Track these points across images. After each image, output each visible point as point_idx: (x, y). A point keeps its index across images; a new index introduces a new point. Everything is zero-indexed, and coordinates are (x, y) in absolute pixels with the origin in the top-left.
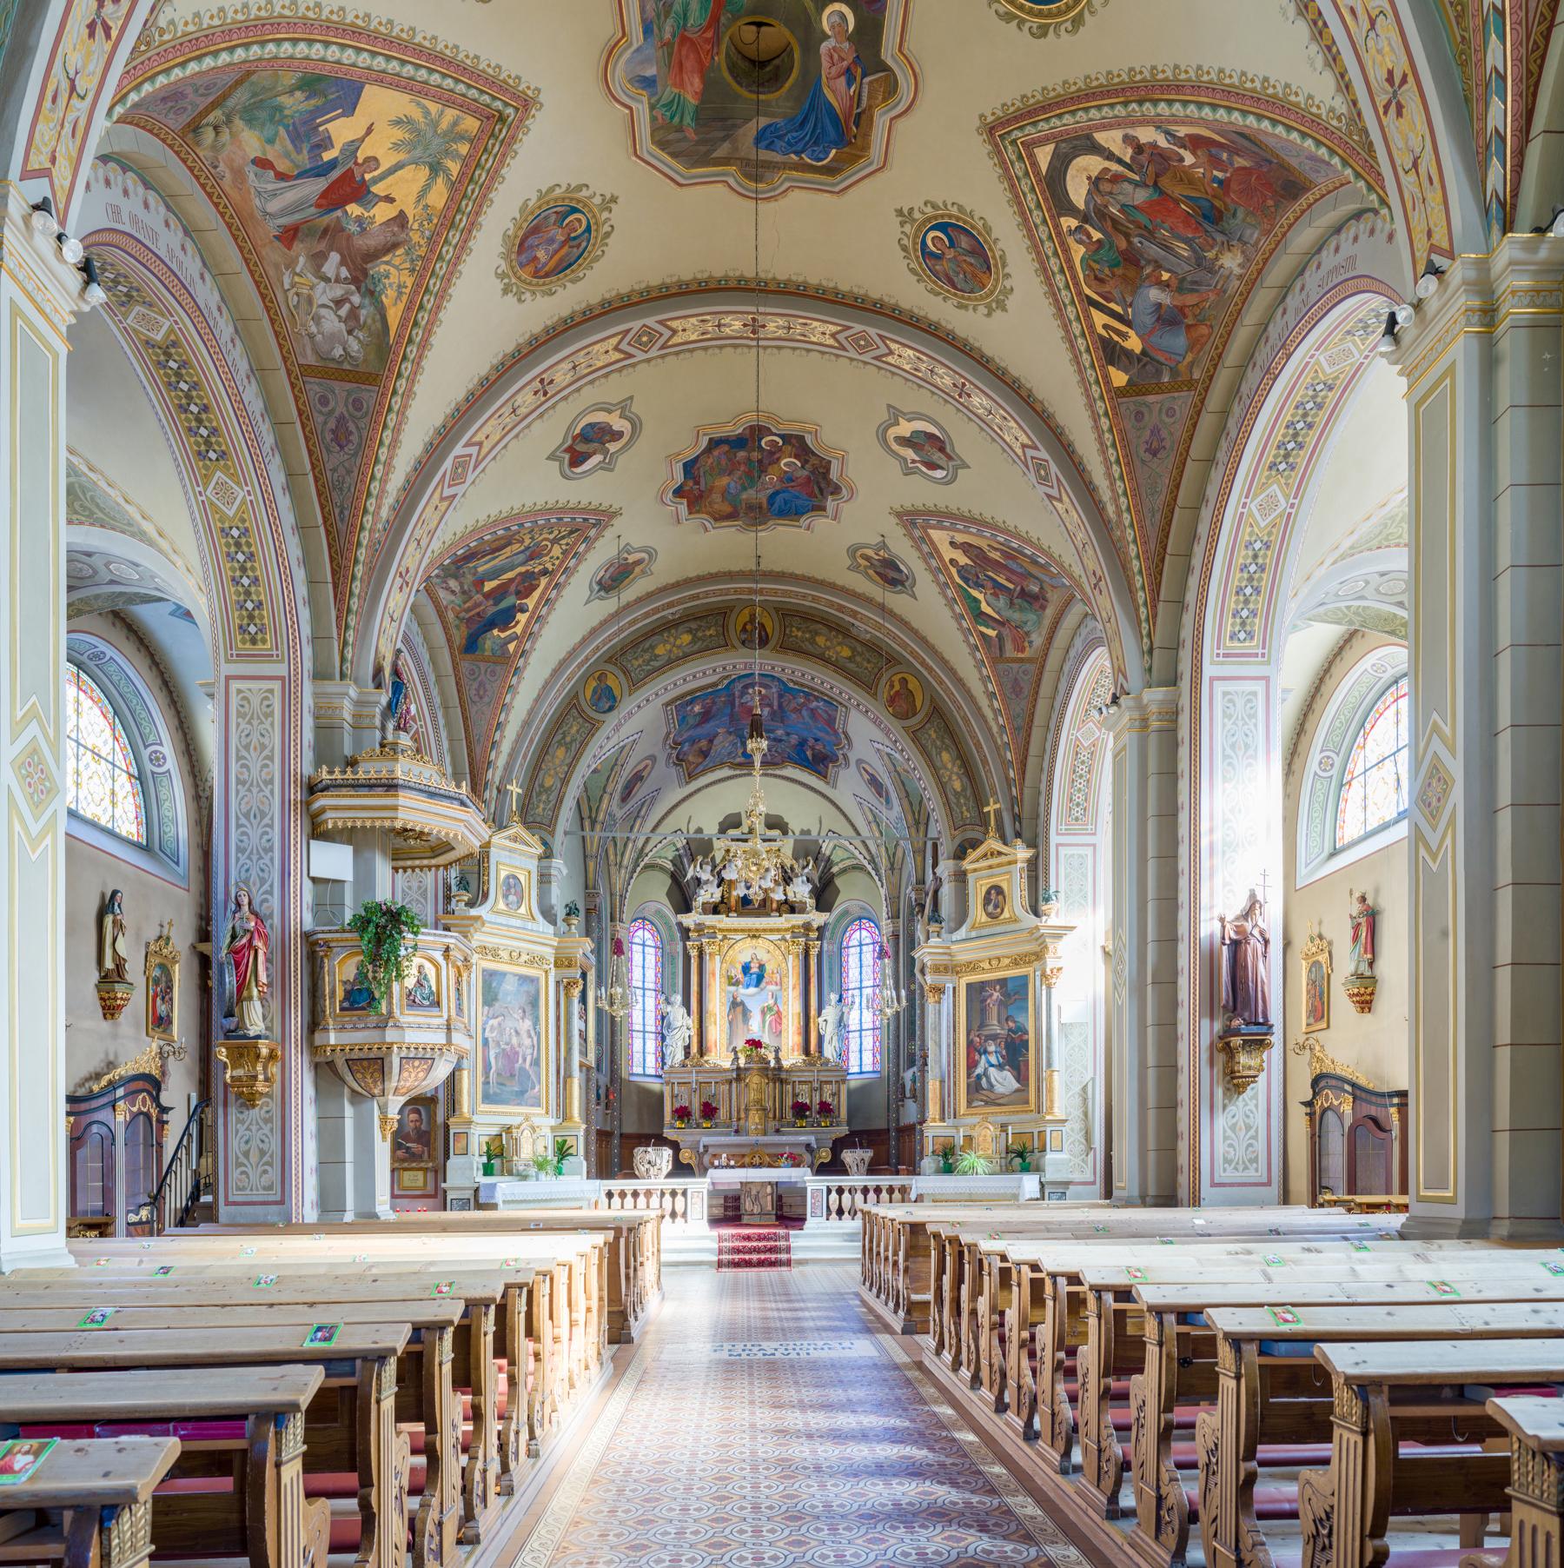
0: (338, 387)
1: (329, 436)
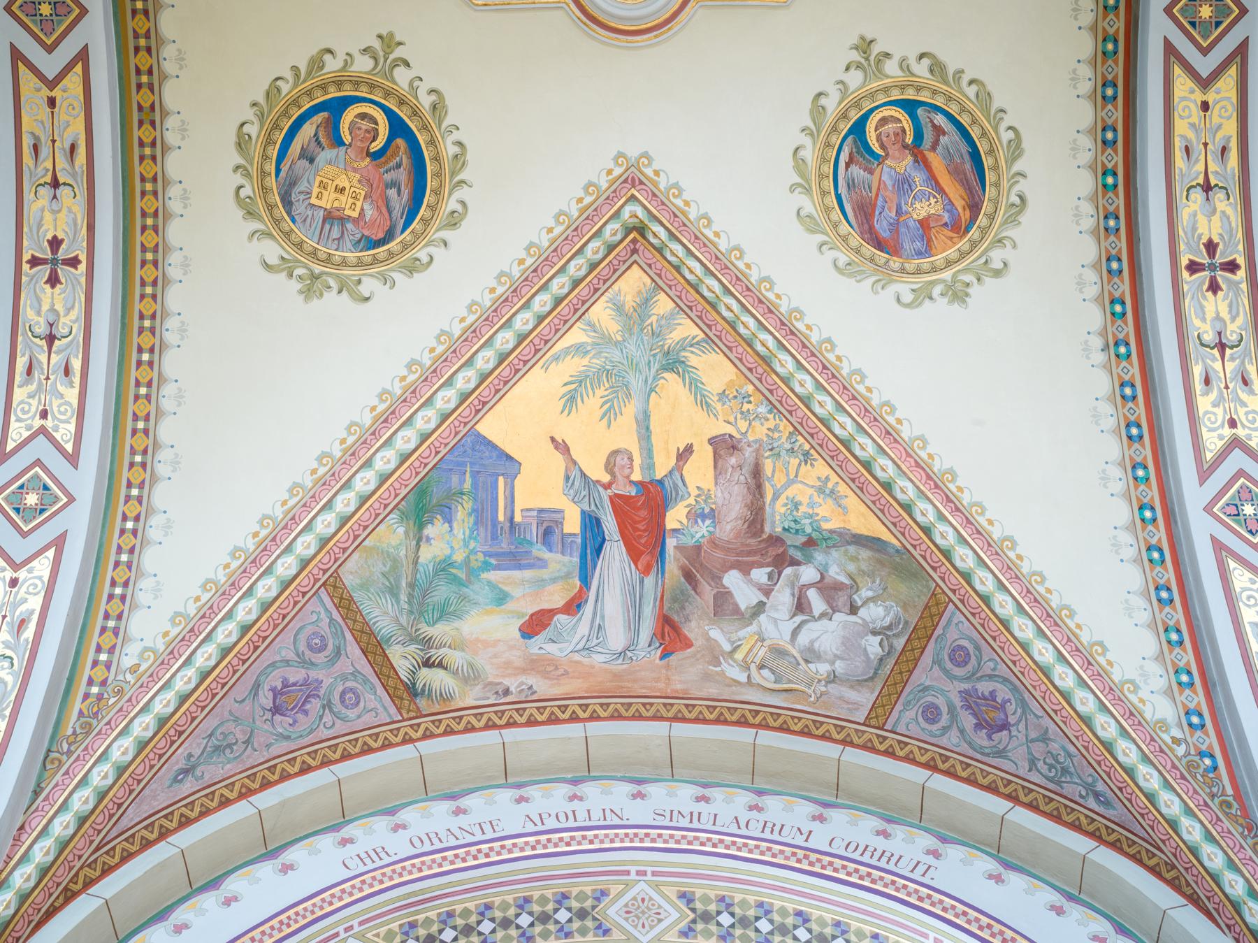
0: (921, 676)
1: (981, 739)
